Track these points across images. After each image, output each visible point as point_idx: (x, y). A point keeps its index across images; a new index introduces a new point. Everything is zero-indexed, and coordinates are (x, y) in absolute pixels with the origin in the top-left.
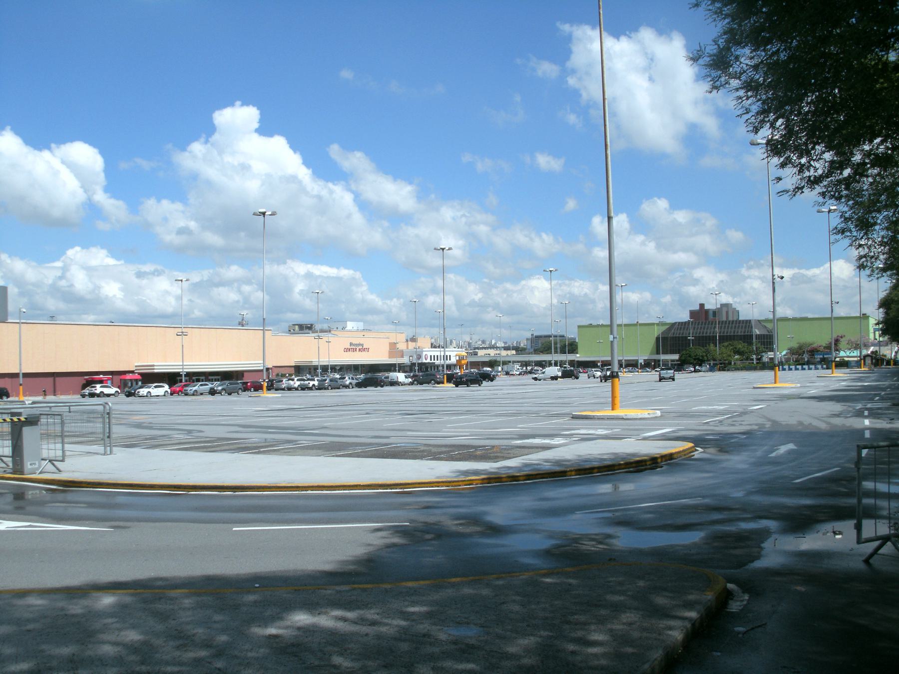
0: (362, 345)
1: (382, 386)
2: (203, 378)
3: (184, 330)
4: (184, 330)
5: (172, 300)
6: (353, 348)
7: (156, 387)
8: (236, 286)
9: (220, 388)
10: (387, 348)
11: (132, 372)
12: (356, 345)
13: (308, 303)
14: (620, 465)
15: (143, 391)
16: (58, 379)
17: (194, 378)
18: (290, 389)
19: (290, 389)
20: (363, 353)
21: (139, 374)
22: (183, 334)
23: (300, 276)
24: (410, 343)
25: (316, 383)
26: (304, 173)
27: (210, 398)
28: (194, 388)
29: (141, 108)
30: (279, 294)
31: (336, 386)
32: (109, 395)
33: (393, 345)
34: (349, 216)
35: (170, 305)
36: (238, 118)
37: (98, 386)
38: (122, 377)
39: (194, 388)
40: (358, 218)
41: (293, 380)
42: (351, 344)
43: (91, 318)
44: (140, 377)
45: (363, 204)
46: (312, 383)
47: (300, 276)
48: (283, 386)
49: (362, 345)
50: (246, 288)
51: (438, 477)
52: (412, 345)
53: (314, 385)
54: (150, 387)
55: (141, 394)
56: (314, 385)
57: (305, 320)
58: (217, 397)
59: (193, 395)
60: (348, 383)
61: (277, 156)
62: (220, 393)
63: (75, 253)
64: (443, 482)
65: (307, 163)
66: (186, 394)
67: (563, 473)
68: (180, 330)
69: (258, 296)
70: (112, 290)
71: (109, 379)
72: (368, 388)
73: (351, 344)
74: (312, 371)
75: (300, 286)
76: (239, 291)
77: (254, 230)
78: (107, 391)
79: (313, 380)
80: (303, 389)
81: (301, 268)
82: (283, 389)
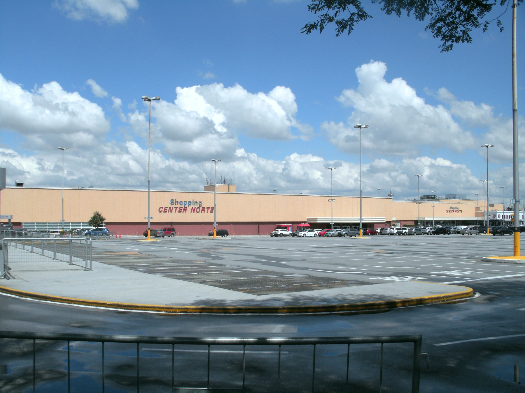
0: (458, 208)
1: (449, 234)
2: (339, 227)
3: (333, 198)
4: (333, 198)
5: (352, 181)
6: (452, 210)
7: (309, 231)
8: (390, 172)
9: (344, 233)
10: (474, 210)
11: (305, 222)
12: (454, 208)
13: (432, 183)
14: (343, 306)
15: (302, 234)
16: (260, 226)
17: (343, 227)
18: (392, 234)
19: (392, 234)
20: (458, 213)
21: (309, 223)
22: (332, 200)
23: (425, 166)
24: (489, 207)
25: (407, 231)
26: (418, 102)
27: (338, 239)
28: (332, 233)
29: (133, 61)
30: (415, 178)
31: (419, 233)
32: (286, 235)
33: (477, 208)
34: (448, 127)
35: (351, 184)
36: (373, 70)
37: (279, 230)
38: (299, 225)
39: (332, 233)
40: (454, 127)
41: (393, 229)
42: (450, 208)
43: (304, 192)
44: (309, 225)
45: (456, 119)
46: (404, 231)
47: (425, 166)
48: (388, 232)
49: (458, 208)
50: (393, 174)
51: (166, 305)
52: (490, 209)
53: (405, 232)
54: (305, 231)
55: (300, 235)
56: (405, 232)
57: (428, 193)
58: (342, 238)
59: (332, 236)
60: (427, 231)
61: (402, 91)
62: (344, 236)
63: (294, 156)
64: (163, 308)
65: (419, 94)
66: (328, 236)
67: (306, 309)
68: (330, 198)
69: (404, 177)
70: (317, 175)
71: (290, 226)
72: (440, 235)
73: (450, 208)
74: (425, 224)
75: (426, 172)
76: (389, 175)
77: (392, 140)
78: (284, 233)
79: (406, 229)
80: (399, 235)
81: (426, 161)
82: (388, 234)
